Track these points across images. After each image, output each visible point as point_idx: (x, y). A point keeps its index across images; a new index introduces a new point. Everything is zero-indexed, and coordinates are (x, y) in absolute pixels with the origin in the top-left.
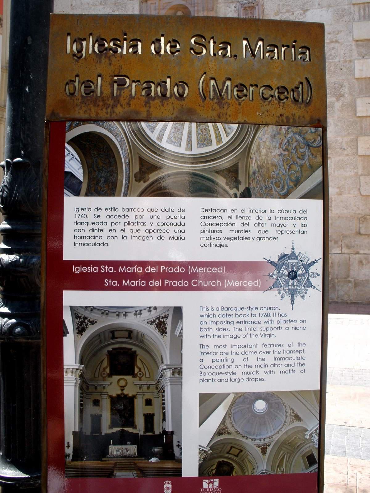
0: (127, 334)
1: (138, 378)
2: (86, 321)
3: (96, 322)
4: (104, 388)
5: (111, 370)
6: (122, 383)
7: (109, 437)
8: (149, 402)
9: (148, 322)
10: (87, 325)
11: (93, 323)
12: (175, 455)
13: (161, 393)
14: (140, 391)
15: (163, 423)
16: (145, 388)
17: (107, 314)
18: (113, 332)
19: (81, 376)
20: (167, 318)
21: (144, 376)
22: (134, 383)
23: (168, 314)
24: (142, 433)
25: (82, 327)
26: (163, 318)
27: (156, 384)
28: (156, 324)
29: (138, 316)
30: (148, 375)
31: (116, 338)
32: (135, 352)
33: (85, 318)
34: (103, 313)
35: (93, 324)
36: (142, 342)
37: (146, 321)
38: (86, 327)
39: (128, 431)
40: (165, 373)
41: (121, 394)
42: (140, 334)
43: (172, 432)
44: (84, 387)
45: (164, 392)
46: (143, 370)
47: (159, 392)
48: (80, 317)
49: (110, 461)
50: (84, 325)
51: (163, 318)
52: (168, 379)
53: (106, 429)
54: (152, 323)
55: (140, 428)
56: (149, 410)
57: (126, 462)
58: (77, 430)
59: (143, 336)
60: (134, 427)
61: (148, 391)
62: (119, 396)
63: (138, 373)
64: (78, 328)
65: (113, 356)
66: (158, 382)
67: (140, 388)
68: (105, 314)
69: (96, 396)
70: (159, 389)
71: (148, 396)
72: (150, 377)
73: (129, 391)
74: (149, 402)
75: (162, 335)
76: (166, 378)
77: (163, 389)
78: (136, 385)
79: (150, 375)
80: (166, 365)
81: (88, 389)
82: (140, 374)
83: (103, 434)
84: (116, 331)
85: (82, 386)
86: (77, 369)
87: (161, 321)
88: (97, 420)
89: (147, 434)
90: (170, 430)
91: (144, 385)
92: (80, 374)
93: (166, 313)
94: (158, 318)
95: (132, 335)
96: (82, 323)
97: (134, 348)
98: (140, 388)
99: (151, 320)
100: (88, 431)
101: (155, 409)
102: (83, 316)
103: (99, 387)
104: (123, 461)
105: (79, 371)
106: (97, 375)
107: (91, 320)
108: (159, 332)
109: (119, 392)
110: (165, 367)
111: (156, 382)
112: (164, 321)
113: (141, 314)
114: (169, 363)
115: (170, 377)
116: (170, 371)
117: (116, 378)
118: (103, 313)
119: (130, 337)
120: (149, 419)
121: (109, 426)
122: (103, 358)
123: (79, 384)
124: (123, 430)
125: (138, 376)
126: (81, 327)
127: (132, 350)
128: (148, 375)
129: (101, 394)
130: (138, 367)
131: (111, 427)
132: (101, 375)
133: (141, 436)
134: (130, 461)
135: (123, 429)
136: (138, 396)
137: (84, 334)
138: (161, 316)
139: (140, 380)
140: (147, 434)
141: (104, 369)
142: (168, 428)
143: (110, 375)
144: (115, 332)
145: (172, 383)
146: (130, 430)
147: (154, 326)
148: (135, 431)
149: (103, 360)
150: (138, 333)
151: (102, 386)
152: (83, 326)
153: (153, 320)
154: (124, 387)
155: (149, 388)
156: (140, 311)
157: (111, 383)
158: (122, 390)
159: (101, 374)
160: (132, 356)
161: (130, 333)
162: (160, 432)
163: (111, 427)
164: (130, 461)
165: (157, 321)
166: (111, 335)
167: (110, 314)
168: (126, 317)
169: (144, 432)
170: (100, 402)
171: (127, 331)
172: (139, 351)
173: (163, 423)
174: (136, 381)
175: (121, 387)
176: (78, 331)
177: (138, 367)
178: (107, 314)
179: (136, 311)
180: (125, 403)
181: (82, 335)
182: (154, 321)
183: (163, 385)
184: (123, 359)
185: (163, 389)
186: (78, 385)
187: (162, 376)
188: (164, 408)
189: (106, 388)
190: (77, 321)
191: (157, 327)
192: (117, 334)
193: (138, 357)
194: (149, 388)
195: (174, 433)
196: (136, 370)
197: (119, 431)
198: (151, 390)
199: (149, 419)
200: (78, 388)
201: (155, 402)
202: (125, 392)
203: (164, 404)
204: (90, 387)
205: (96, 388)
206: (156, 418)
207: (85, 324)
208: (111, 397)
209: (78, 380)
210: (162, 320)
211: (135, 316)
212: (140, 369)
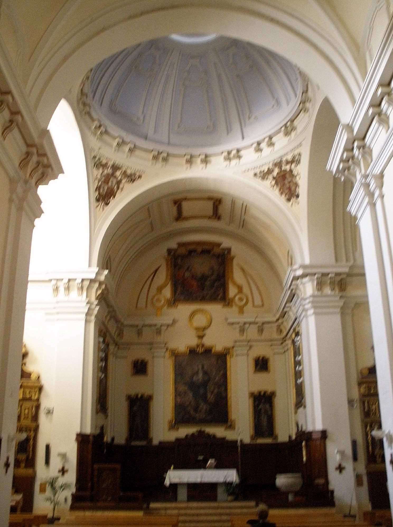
0: (208, 207)
1: (235, 309)
2: (118, 173)
3: (140, 177)
4: (159, 332)
5: (174, 291)
6: (200, 320)
7: (164, 447)
8: (262, 365)
9: (255, 175)
10: (119, 183)
11: (132, 178)
12: (336, 494)
13: (289, 342)
14: (242, 338)
15: (296, 413)
16: (252, 332)
17: (165, 160)
18: (178, 203)
19: (103, 299)
20: (298, 162)
21: (250, 304)
22: (226, 319)
23: (300, 155)
24: (247, 440)
25: (108, 188)
26: (287, 162)
27: (278, 320)
28: (274, 178)
29: (234, 162)
30: (258, 301)
31: (186, 219)
32: (229, 250)
33: (115, 168)
34: (155, 158)
35: (133, 181)
36: (243, 224)
37: (252, 173)
38: (118, 188)
39: (214, 436)
40: (301, 287)
41: (198, 346)
42: (238, 206)
43: (324, 434)
44: (113, 328)
45: (297, 334)
46: (246, 290)
47: (284, 340)
48: (105, 166)
49: (169, 512)
50: (112, 182)
51: (287, 162)
52: (308, 301)
53: (162, 430)
54: (264, 175)
55: (241, 429)
56: (262, 383)
57: (211, 515)
58: (88, 430)
59: (245, 209)
60: (231, 426)
61: (260, 338)
62: (192, 352)
63: (235, 296)
64: (98, 188)
65: (179, 259)
66: (284, 314)
67: (242, 331)
68: (161, 159)
69: (139, 353)
70: (285, 333)
71: (260, 350)
72: (263, 305)
73: (217, 339)
74: (262, 365)
75: (289, 200)
76: (305, 299)
77: (294, 330)
78: (233, 324)
79: (262, 301)
80: (303, 267)
81: (120, 334)
82: (241, 299)
83: (156, 442)
84: (185, 199)
85: (103, 323)
86: (92, 281)
87: (285, 171)
88: (140, 407)
89: (261, 441)
90: (319, 426)
91: (250, 323)
92: (99, 292)
93: (296, 152)
94: (278, 164)
95: (221, 210)
96: (107, 179)
97: (226, 243)
98: (242, 331)
99: (262, 170)
100: (118, 432)
101: (277, 382)
102: (110, 164)
103: (146, 332)
104: (202, 511)
105: (97, 285)
106: (142, 302)
107: (129, 172)
108: (282, 194)
109: (193, 341)
110: (299, 272)
111: (278, 316)
112: (291, 171)
113: (239, 157)
114: (307, 261)
115: (313, 296)
116: (313, 281)
117: (184, 310)
118: (155, 158)
119: (216, 215)
120: (263, 403)
121: (170, 422)
122: (157, 267)
123: (96, 316)
124: (201, 433)
125: (236, 305)
126: (106, 188)
127: (222, 246)
128: (258, 301)
129: (151, 345)
130: (235, 284)
131: (174, 425)
132: (152, 303)
133: (243, 446)
134: (219, 511)
135: (203, 429)
136: (237, 351)
137: (113, 202)
138: (284, 159)
139: (241, 310)
140: (261, 441)
141: (160, 289)
142: (314, 423)
143: (173, 302)
144: (185, 205)
145: (319, 310)
146: (219, 431)
147: (269, 182)
148: (230, 435)
149: (156, 271)
150: (233, 202)
151: (153, 328)
152: (110, 184)
153: (266, 170)
154: (204, 329)
155: (261, 330)
156: (238, 151)
157: (174, 322)
158: (201, 337)
159: (152, 299)
160: (223, 258)
161: (216, 205)
162: (290, 437)
163: (174, 425)
164: (219, 511)
165: (276, 171)
166: (174, 210)
167: (171, 160)
168: (208, 165)
169: (253, 438)
170: (149, 368)
171: (210, 199)
172: (238, 250)
173: (296, 413)
174: (232, 314)
175: (197, 329)
176: (99, 193)
177: (235, 284)
178: (165, 160)
179: (229, 153)
180: (205, 368)
181: (107, 204)
182: (270, 171)
183: (296, 319)
184: (201, 266)
185: (294, 330)
186: (93, 318)
187: (291, 299)
188: (298, 374)
189: (162, 333)
190: (98, 173)
191: (277, 183)
192: (187, 208)
193: (235, 262)
194: (261, 330)
195: (329, 434)
196: (232, 291)
197: (193, 435)
198: (265, 335)
199: (263, 403)
200: (92, 326)
201: (275, 364)
202: (208, 341)
203: (298, 363)
204: (126, 332)
205: (139, 333)
206: (278, 403)
207: (115, 182)
208: (175, 355)
209: (93, 306)
210: (288, 167)
211: (227, 162)
212: (240, 289)
